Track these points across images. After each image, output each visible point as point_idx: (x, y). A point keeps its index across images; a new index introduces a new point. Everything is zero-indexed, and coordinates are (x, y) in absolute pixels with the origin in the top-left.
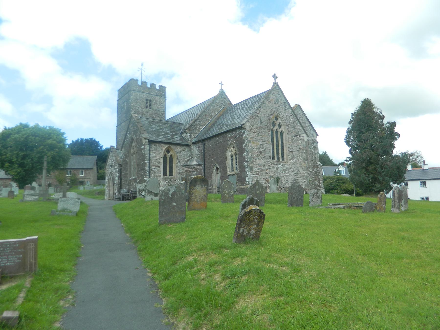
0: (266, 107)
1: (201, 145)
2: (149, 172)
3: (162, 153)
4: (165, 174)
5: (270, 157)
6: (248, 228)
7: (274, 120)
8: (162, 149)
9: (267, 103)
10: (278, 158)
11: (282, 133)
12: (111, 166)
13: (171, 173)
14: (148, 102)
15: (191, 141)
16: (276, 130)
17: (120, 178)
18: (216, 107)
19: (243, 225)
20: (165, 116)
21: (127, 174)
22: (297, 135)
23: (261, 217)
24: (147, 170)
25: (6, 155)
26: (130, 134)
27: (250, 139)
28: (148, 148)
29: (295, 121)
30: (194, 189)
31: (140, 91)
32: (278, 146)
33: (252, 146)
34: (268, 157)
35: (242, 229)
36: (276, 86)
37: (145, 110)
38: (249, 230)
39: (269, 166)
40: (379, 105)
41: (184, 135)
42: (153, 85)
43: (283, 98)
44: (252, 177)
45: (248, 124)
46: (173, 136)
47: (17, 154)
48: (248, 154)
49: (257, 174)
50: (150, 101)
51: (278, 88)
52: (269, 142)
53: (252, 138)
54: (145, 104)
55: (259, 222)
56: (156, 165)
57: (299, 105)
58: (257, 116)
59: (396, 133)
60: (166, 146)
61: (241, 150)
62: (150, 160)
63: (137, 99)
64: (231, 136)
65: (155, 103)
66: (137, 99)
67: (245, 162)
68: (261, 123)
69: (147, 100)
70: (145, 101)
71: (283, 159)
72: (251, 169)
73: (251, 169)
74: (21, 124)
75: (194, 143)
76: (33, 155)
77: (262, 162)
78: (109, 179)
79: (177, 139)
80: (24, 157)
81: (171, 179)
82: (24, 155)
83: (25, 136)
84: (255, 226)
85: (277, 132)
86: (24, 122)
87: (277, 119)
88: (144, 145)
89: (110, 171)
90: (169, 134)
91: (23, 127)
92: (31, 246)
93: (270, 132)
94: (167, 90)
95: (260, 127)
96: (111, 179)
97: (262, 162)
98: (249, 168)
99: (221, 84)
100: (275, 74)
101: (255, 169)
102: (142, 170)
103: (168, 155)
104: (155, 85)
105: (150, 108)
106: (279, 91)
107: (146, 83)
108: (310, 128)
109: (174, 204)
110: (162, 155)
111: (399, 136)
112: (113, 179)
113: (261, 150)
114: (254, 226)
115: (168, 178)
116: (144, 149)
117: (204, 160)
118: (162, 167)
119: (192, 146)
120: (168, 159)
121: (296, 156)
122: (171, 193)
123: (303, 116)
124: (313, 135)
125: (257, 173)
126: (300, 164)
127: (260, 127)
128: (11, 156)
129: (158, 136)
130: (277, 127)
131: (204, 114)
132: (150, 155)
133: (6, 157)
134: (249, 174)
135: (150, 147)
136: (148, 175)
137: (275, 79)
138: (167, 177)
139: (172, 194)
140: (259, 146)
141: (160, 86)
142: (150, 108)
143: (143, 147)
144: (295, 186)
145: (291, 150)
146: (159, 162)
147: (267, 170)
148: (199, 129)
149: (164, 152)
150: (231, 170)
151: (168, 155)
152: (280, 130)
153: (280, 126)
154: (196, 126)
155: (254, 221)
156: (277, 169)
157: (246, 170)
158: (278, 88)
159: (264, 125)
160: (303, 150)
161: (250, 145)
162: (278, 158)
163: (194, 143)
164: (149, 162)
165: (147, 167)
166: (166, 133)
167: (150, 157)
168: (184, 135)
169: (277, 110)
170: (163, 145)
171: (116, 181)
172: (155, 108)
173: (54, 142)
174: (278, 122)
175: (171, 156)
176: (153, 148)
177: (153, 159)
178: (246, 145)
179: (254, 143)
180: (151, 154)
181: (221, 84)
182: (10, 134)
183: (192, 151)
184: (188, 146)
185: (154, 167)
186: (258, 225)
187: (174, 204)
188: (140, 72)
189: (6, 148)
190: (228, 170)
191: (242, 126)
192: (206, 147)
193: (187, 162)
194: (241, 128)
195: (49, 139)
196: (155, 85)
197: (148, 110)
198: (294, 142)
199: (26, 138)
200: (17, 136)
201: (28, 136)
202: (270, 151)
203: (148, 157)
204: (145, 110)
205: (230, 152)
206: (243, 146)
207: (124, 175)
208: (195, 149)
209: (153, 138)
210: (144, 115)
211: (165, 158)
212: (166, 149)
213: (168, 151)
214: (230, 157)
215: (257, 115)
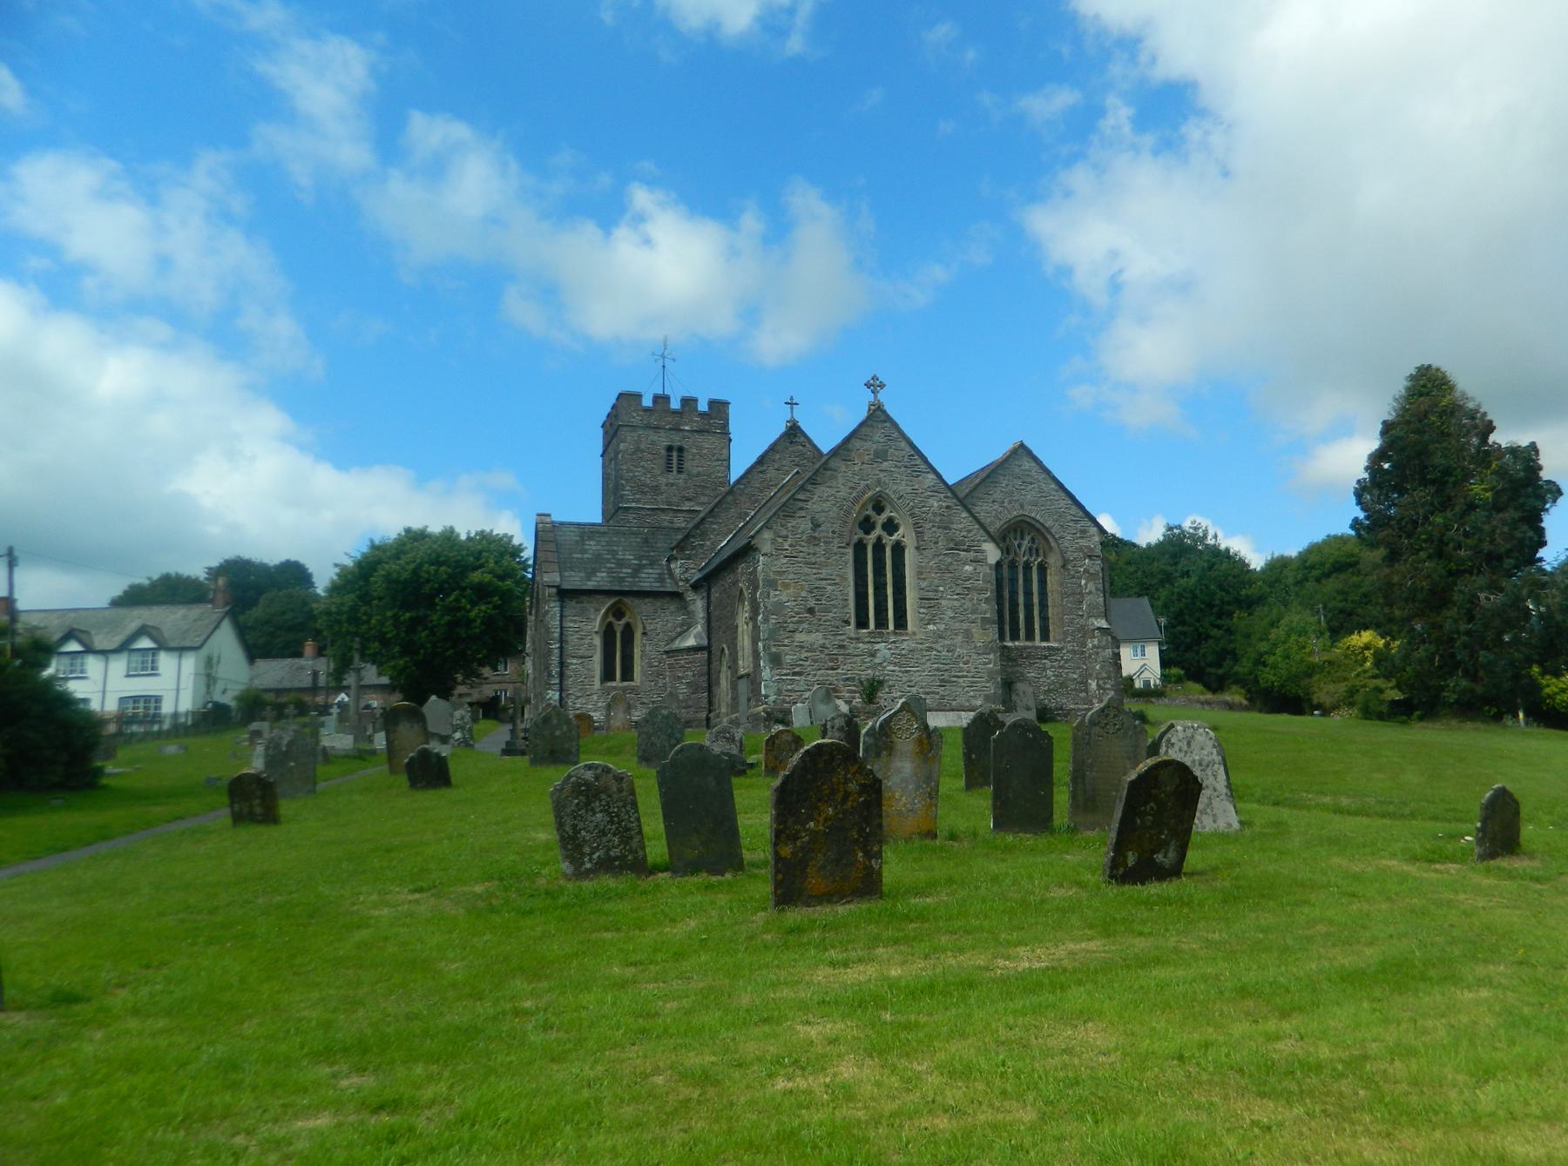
2: (562, 675)
4: (608, 675)
5: (847, 623)
10: (881, 622)
11: (899, 549)
13: (627, 674)
14: (675, 454)
15: (687, 581)
22: (957, 546)
24: (555, 670)
25: (368, 622)
27: (772, 576)
31: (648, 427)
32: (880, 588)
34: (838, 623)
36: (877, 415)
37: (663, 480)
39: (842, 647)
40: (1472, 383)
43: (903, 444)
46: (637, 570)
47: (396, 617)
49: (795, 674)
50: (681, 449)
54: (663, 462)
56: (580, 653)
57: (1022, 445)
59: (1549, 482)
63: (638, 450)
66: (638, 450)
68: (816, 526)
69: (670, 449)
70: (663, 452)
71: (901, 622)
73: (776, 661)
74: (408, 531)
76: (435, 617)
77: (816, 638)
79: (648, 581)
80: (414, 624)
81: (624, 690)
82: (411, 619)
83: (412, 566)
84: (257, 801)
85: (879, 547)
86: (416, 525)
91: (415, 537)
93: (850, 551)
94: (733, 412)
97: (816, 638)
99: (791, 404)
101: (788, 659)
103: (619, 626)
104: (695, 400)
108: (1074, 510)
111: (1557, 492)
113: (812, 603)
114: (257, 801)
115: (615, 688)
118: (598, 658)
119: (690, 596)
121: (950, 613)
122: (285, 742)
124: (1084, 532)
126: (968, 635)
128: (382, 623)
129: (591, 574)
130: (878, 531)
133: (370, 629)
135: (562, 607)
138: (614, 684)
141: (712, 403)
145: (931, 595)
146: (591, 645)
147: (832, 660)
148: (714, 544)
151: (619, 626)
152: (889, 541)
153: (891, 527)
154: (704, 536)
156: (873, 654)
160: (981, 591)
161: (772, 593)
162: (881, 622)
165: (555, 659)
166: (621, 564)
169: (879, 482)
172: (695, 471)
173: (487, 577)
175: (628, 625)
177: (573, 639)
179: (786, 586)
181: (791, 404)
182: (380, 562)
189: (369, 603)
193: (673, 640)
195: (475, 568)
196: (695, 400)
197: (672, 477)
198: (943, 570)
199: (415, 572)
200: (393, 566)
201: (421, 565)
203: (556, 635)
209: (575, 580)
213: (618, 612)
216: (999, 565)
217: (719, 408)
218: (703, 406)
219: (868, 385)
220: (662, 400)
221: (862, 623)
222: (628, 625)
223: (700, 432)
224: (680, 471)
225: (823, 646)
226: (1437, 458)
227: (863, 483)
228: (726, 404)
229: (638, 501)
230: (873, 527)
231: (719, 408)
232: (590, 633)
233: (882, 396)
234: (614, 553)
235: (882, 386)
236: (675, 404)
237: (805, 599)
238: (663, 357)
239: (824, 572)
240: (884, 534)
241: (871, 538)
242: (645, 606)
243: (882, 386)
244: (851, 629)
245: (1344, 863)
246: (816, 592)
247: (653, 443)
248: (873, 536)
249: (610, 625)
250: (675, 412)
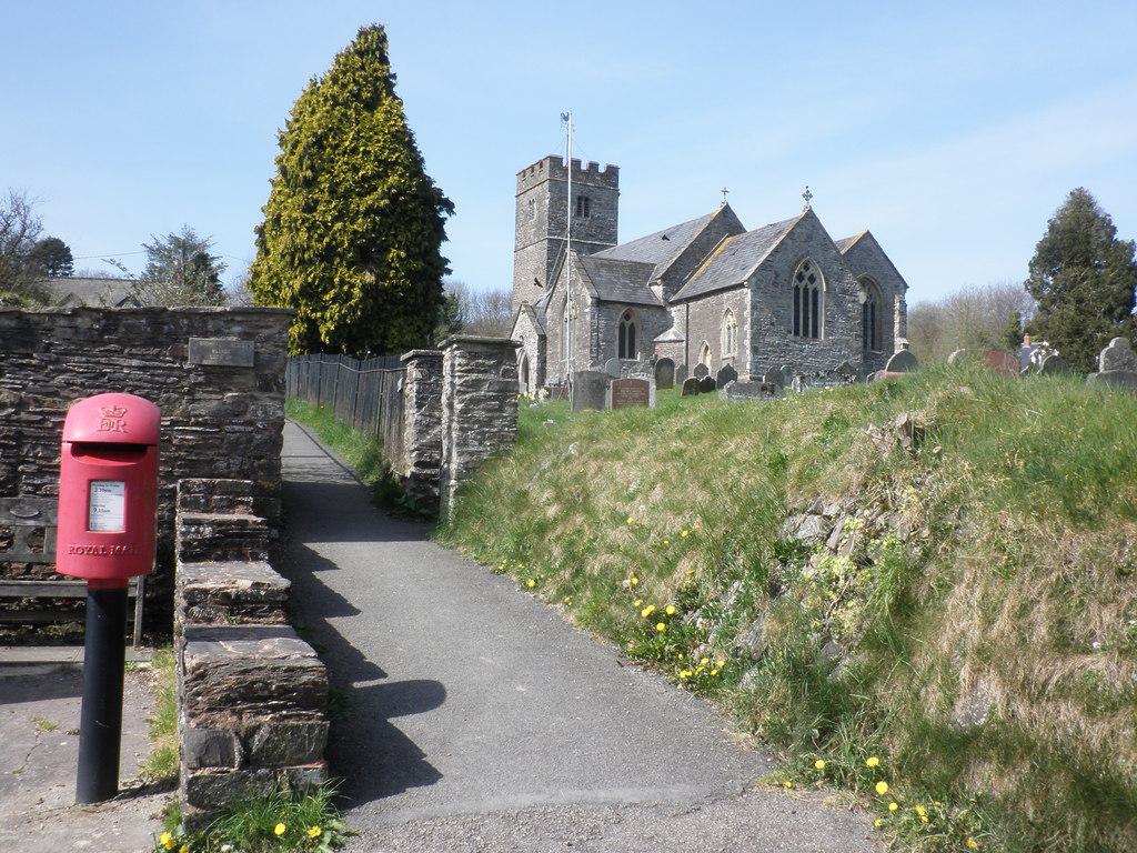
11: (815, 293)
32: (806, 312)
50: (587, 199)
52: (789, 307)
71: (815, 335)
130: (806, 281)
175: (632, 324)
211: (622, 327)
213: (627, 317)
216: (865, 305)
217: (612, 172)
218: (602, 169)
221: (797, 333)
222: (632, 324)
224: (586, 215)
226: (1077, 240)
228: (616, 169)
231: (612, 172)
242: (643, 312)
243: (811, 196)
244: (791, 336)
245: (451, 500)
248: (804, 283)
250: (584, 172)
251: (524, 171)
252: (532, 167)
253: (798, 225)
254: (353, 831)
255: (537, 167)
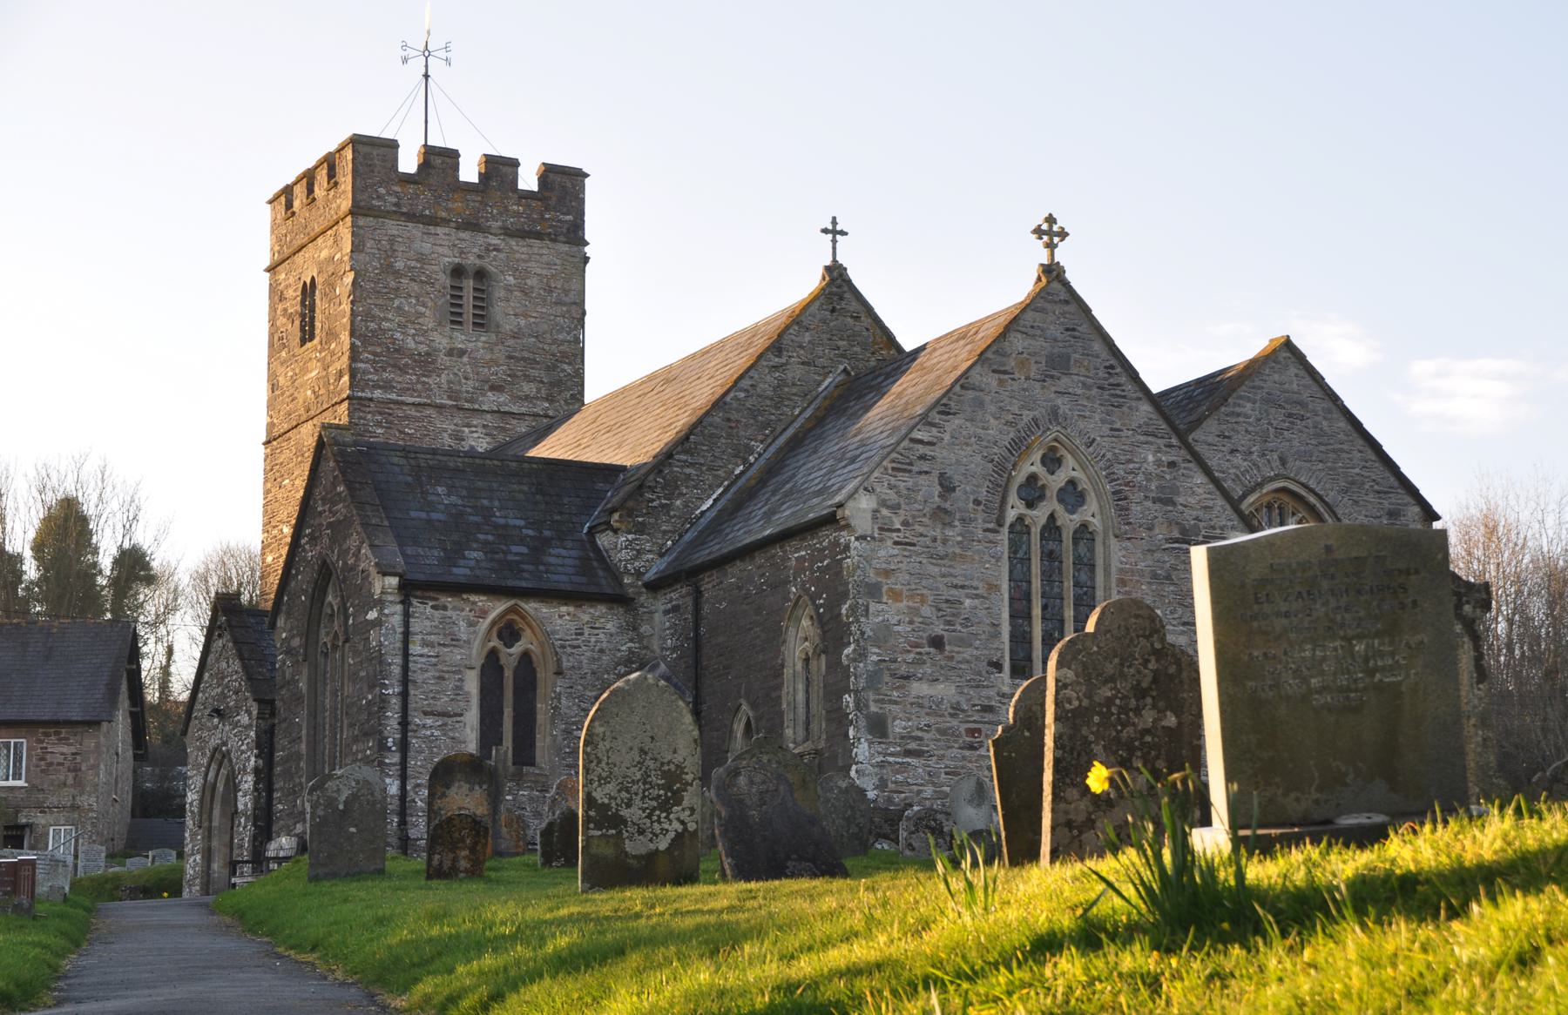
0: (981, 404)
1: (678, 595)
3: (477, 643)
5: (998, 666)
6: (451, 856)
7: (1038, 468)
8: (471, 624)
9: (992, 381)
12: (218, 712)
14: (469, 284)
15: (638, 574)
16: (1043, 521)
17: (265, 776)
18: (795, 372)
19: (439, 849)
20: (579, 376)
21: (299, 757)
23: (478, 833)
26: (313, 539)
27: (872, 577)
28: (397, 621)
29: (1172, 464)
30: (444, 795)
33: (886, 612)
35: (437, 857)
37: (441, 341)
38: (455, 860)
41: (604, 540)
42: (499, 169)
43: (1097, 346)
44: (881, 765)
45: (865, 503)
46: (539, 547)
48: (861, 655)
49: (908, 753)
50: (481, 274)
51: (1063, 295)
52: (993, 588)
53: (887, 573)
55: (476, 843)
58: (923, 457)
60: (498, 607)
61: (833, 634)
62: (405, 681)
64: (801, 560)
65: (508, 289)
67: (849, 691)
68: (947, 487)
69: (458, 272)
70: (445, 280)
72: (878, 727)
73: (878, 727)
75: (654, 587)
77: (945, 691)
78: (208, 791)
84: (465, 853)
87: (1052, 461)
88: (380, 603)
89: (214, 742)
90: (522, 541)
92: (25, 873)
94: (591, 189)
95: (941, 515)
96: (220, 787)
97: (945, 691)
98: (862, 723)
99: (834, 232)
100: (1051, 220)
101: (898, 727)
102: (367, 735)
105: (481, 323)
106: (1072, 308)
107: (450, 157)
108: (1379, 471)
109: (353, 830)
110: (476, 655)
112: (233, 786)
113: (939, 629)
114: (465, 853)
116: (378, 623)
117: (697, 689)
118: (472, 716)
120: (508, 674)
122: (343, 798)
123: (1322, 405)
125: (913, 746)
127: (941, 515)
131: (717, 418)
132: (406, 654)
134: (862, 750)
135: (407, 616)
136: (394, 759)
137: (1051, 246)
139: (345, 802)
140: (926, 611)
142: (481, 323)
143: (372, 615)
144: (831, 790)
149: (487, 638)
150: (801, 733)
152: (1069, 522)
153: (1072, 495)
154: (672, 489)
155: (462, 840)
157: (851, 733)
158: (1063, 295)
159: (961, 501)
161: (873, 607)
163: (654, 587)
164: (404, 695)
166: (506, 535)
167: (405, 668)
168: (604, 540)
170: (480, 600)
171: (244, 802)
174: (1059, 479)
175: (526, 656)
176: (425, 615)
177: (422, 675)
178: (853, 609)
179: (896, 596)
180: (415, 649)
181: (834, 232)
183: (645, 629)
184: (619, 600)
185: (429, 721)
186: (473, 850)
187: (353, 830)
188: (417, 66)
190: (789, 732)
191: (834, 514)
192: (706, 609)
194: (831, 520)
196: (514, 164)
202: (997, 635)
203: (396, 670)
204: (441, 341)
205: (800, 639)
206: (844, 611)
207: (285, 760)
208: (657, 617)
210: (438, 372)
211: (491, 666)
212: (493, 623)
213: (509, 632)
214: (799, 666)
215: (922, 449)
217: (564, 185)
218: (528, 180)
219: (1038, 232)
220: (439, 160)
223: (523, 234)
225: (957, 708)
227: (1027, 415)
229: (387, 386)
230: (1062, 495)
231: (564, 185)
232: (458, 670)
233: (1063, 255)
234: (487, 513)
235: (1063, 234)
236: (469, 172)
237: (926, 622)
238: (427, 53)
239: (959, 569)
240: (1059, 509)
241: (1039, 516)
243: (1063, 234)
246: (948, 608)
247: (422, 259)
249: (493, 655)
250: (407, 179)
251: (288, 191)
252: (309, 177)
253: (777, 346)
254: (1339, 512)
255: (322, 176)
